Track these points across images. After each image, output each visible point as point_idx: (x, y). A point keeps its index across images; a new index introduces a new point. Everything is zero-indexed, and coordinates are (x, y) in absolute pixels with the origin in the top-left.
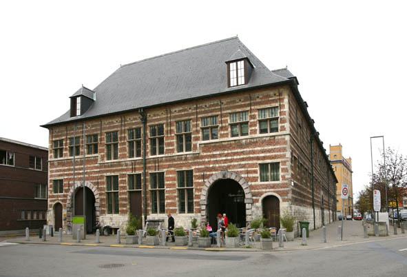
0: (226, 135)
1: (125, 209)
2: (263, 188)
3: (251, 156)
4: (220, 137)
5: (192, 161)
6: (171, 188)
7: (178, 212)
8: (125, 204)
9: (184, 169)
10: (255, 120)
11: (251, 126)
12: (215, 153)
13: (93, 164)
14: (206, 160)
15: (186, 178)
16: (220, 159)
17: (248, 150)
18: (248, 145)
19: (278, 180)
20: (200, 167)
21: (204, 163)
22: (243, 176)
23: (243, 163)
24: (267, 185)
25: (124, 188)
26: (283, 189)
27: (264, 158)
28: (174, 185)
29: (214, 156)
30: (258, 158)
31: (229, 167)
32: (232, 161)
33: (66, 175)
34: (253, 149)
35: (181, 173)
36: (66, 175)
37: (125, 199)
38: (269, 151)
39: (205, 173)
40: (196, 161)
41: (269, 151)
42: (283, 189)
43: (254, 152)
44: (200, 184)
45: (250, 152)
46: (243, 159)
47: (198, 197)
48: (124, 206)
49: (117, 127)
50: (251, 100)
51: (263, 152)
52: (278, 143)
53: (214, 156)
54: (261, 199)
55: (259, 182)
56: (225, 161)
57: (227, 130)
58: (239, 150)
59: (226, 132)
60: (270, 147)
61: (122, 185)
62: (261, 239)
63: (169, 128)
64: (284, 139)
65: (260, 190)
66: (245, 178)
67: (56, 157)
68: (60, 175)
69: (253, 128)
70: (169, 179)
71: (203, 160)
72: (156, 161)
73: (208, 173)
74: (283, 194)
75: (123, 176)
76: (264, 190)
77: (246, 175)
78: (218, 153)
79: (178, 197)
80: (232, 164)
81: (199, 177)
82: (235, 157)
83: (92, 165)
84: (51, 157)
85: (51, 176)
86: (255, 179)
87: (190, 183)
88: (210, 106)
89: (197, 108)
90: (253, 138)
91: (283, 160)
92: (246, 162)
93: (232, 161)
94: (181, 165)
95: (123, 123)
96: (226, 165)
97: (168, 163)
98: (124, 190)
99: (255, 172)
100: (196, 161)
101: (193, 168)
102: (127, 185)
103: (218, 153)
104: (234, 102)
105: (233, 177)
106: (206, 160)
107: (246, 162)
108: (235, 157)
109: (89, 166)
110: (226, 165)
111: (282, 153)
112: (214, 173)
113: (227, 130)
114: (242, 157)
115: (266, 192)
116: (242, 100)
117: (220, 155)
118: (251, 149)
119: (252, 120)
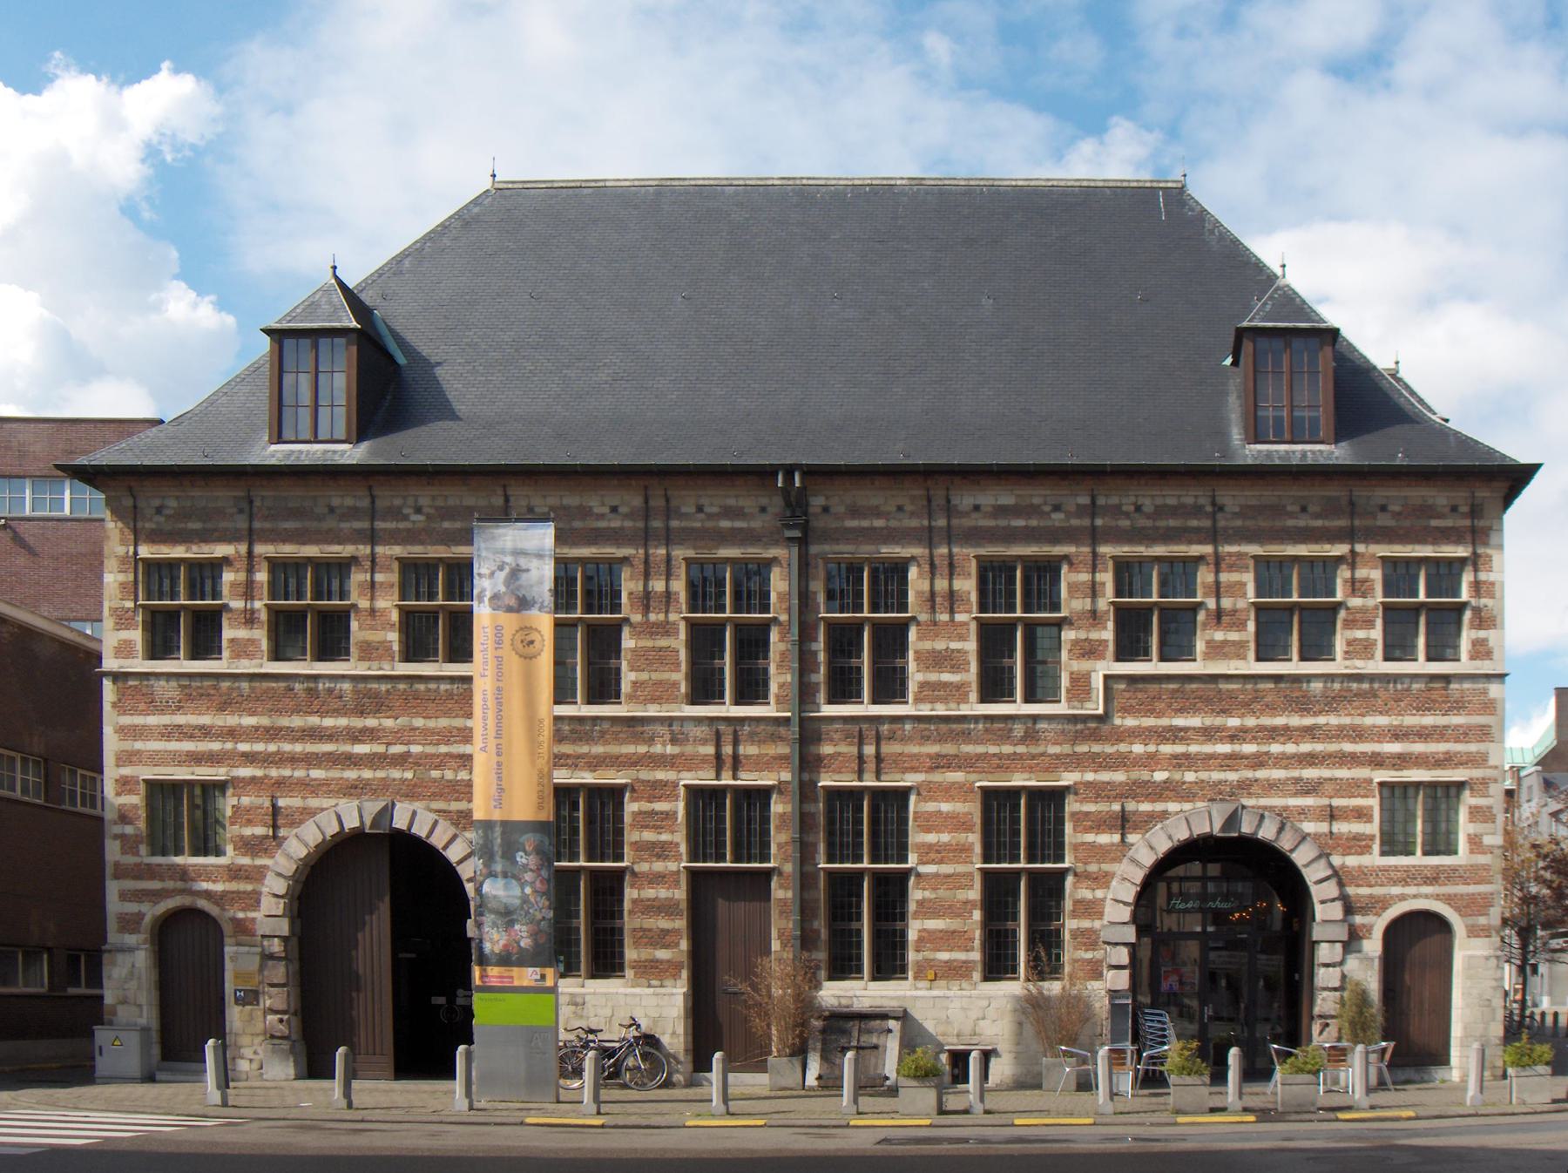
0: (1237, 650)
1: (662, 954)
2: (1395, 883)
3: (1348, 747)
4: (1208, 656)
5: (1067, 749)
6: (944, 865)
7: (977, 976)
8: (665, 932)
9: (1018, 781)
10: (1370, 602)
11: (1349, 624)
12: (1179, 722)
13: (447, 714)
14: (1138, 748)
15: (1023, 825)
16: (1208, 749)
17: (1333, 720)
18: (1331, 703)
19: (1451, 850)
20: (1105, 776)
21: (1121, 761)
22: (1309, 827)
23: (1310, 773)
24: (1407, 869)
25: (661, 851)
26: (1472, 889)
27: (1402, 761)
28: (965, 849)
29: (1176, 735)
30: (1377, 761)
31: (1245, 786)
32: (1259, 761)
33: (250, 758)
34: (1358, 721)
35: (997, 803)
36: (250, 758)
37: (666, 908)
38: (1423, 734)
39: (1131, 806)
40: (1082, 748)
41: (1423, 734)
42: (1472, 889)
43: (1359, 734)
44: (1101, 853)
45: (1341, 733)
46: (1310, 760)
47: (1091, 909)
48: (662, 938)
49: (615, 537)
50: (1352, 515)
51: (1398, 735)
52: (1458, 706)
53: (1176, 735)
54: (1379, 924)
55: (1374, 859)
56: (1231, 761)
57: (1242, 626)
58: (1295, 721)
59: (1234, 636)
60: (1428, 720)
61: (649, 836)
62: (1510, 1071)
63: (941, 584)
64: (1485, 692)
65: (1378, 891)
66: (1316, 837)
67: (1397, 648)
68: (197, 759)
69: (1360, 634)
70: (931, 823)
71: (1123, 747)
72: (859, 729)
73: (1145, 807)
74: (1470, 906)
75: (659, 790)
76: (1396, 890)
77: (1323, 827)
78: (1195, 721)
79: (285, 939)
80: (1261, 774)
81: (1100, 823)
82: (1275, 748)
83: (443, 722)
84: (124, 650)
85: (126, 758)
86: (1358, 844)
87: (1048, 841)
88: (1160, 512)
89: (1093, 510)
90: (1359, 678)
91: (1477, 773)
92: (1326, 773)
93: (1259, 761)
94: (1005, 764)
95: (657, 524)
96: (1232, 776)
97: (934, 749)
98: (657, 866)
99: (1361, 814)
100: (1082, 748)
101: (1067, 779)
102: (680, 838)
103: (1195, 721)
104: (1278, 511)
105: (1267, 832)
106: (1138, 748)
107: (1326, 773)
108: (1275, 748)
109: (419, 722)
110: (1232, 776)
111: (1473, 747)
112: (1173, 807)
113: (1242, 626)
114: (1305, 748)
115: (1403, 898)
116: (1312, 508)
117: (1208, 734)
118: (1347, 720)
119: (1355, 602)
